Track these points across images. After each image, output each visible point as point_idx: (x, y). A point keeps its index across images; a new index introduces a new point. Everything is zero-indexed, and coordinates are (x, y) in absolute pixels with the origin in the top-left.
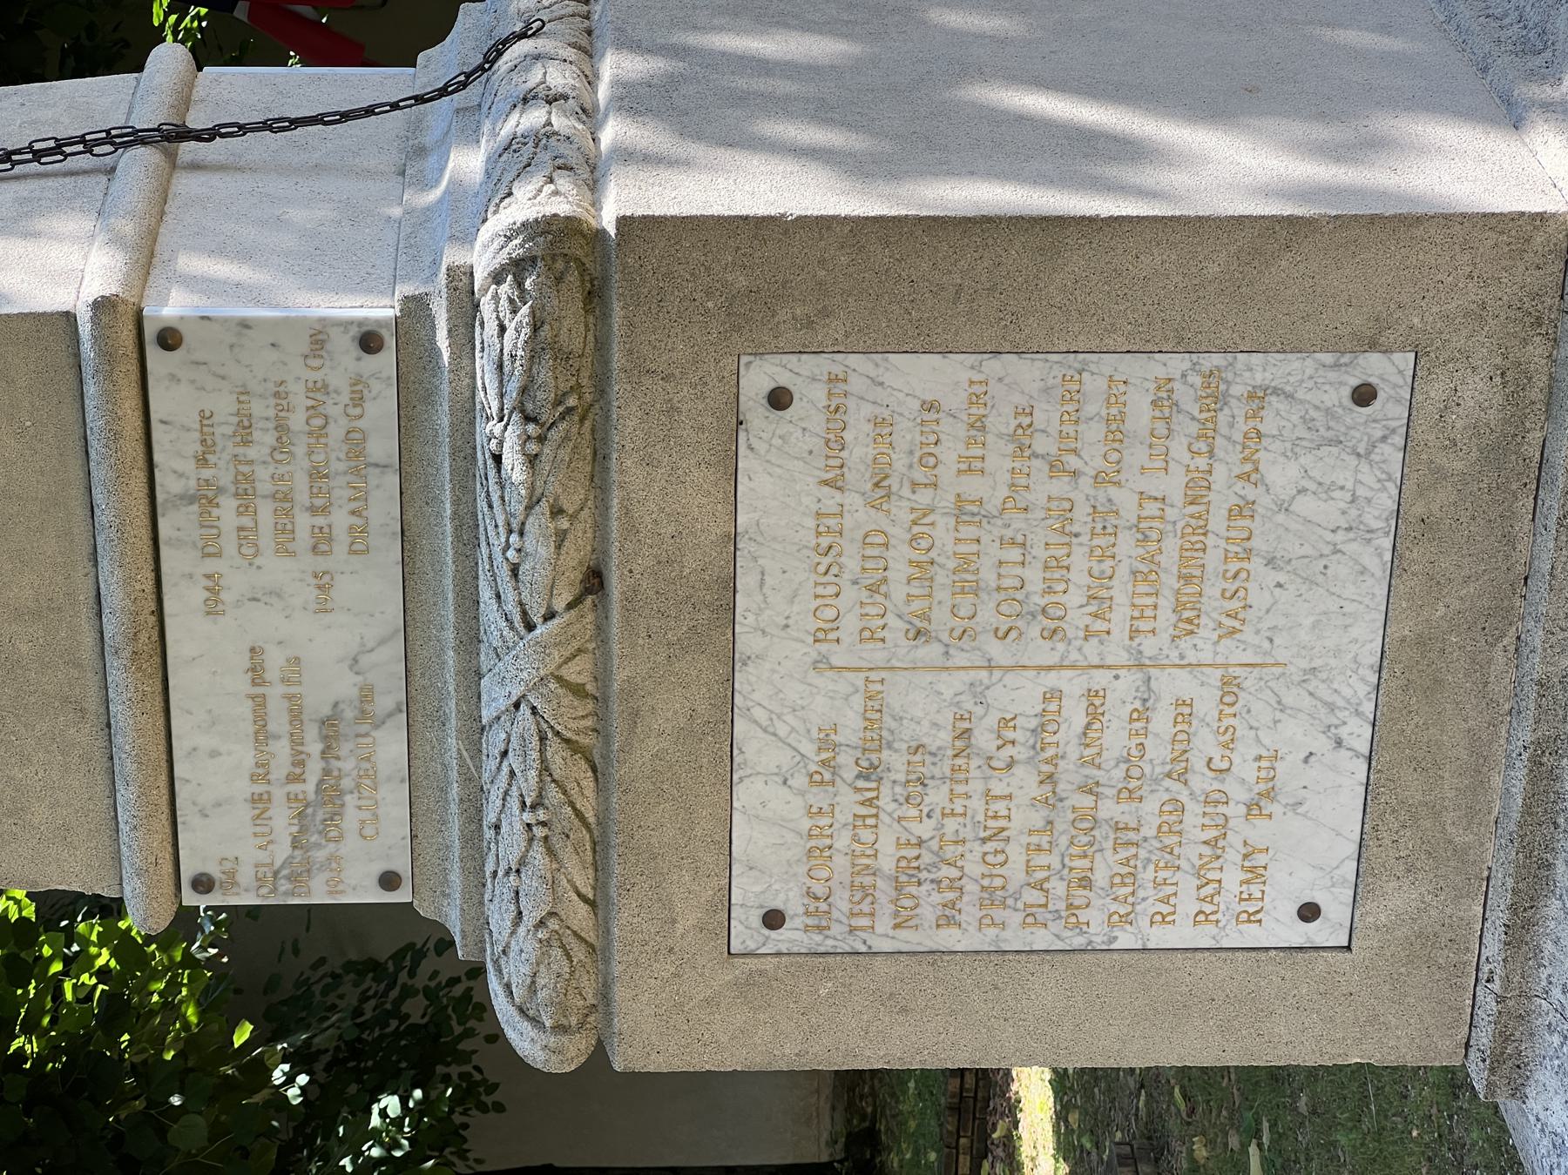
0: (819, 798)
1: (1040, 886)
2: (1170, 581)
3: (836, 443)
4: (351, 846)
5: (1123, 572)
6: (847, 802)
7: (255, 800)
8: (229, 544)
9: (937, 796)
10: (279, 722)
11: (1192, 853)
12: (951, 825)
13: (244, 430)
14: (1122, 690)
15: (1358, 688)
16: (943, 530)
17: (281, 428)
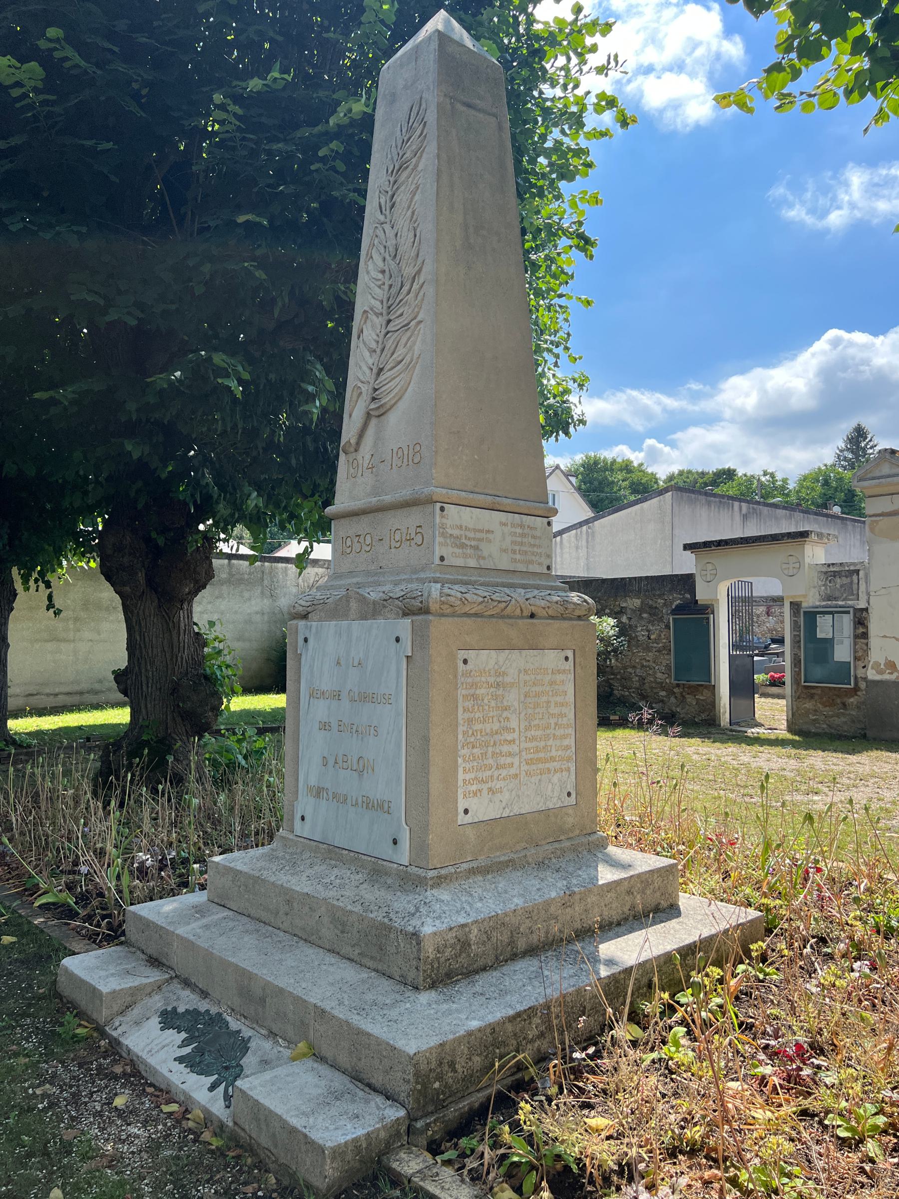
0: (492, 672)
1: (473, 734)
2: (536, 756)
3: (559, 672)
4: (451, 550)
5: (538, 744)
6: (491, 680)
7: (461, 526)
8: (513, 530)
9: (493, 703)
10: (479, 535)
11: (480, 775)
12: (487, 708)
13: (534, 537)
14: (515, 748)
15: (516, 810)
16: (545, 699)
17: (534, 545)
